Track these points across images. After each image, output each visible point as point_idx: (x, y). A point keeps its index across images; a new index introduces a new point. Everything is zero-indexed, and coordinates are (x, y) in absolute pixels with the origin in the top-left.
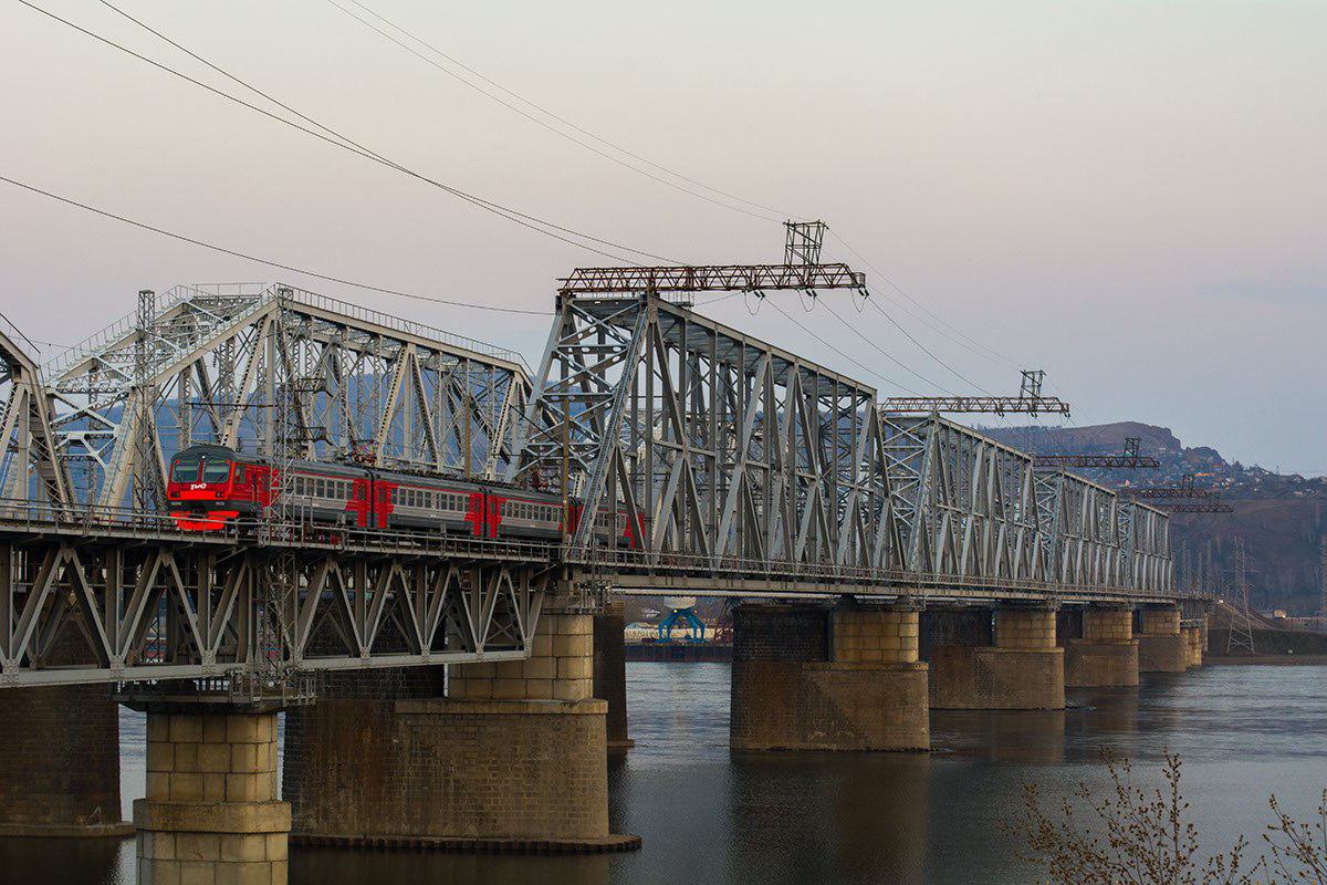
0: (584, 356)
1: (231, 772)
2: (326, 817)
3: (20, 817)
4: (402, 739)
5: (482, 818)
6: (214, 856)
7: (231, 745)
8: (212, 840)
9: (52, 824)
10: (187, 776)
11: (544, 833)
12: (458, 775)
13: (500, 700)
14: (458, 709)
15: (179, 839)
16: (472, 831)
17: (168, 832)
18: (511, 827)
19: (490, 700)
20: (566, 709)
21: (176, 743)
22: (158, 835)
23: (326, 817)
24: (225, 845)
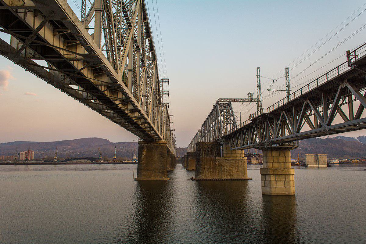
0: (82, 71)
1: (286, 162)
2: (205, 176)
3: (153, 177)
4: (217, 163)
5: (230, 175)
6: (284, 180)
7: (286, 156)
8: (283, 176)
9: (158, 178)
10: (276, 163)
11: (240, 177)
12: (226, 169)
13: (232, 157)
14: (226, 158)
15: (276, 176)
16: (229, 177)
17: (273, 175)
18: (235, 177)
19: (231, 157)
20: (243, 158)
21: (273, 157)
22: (271, 176)
23: (205, 176)
24: (286, 177)
